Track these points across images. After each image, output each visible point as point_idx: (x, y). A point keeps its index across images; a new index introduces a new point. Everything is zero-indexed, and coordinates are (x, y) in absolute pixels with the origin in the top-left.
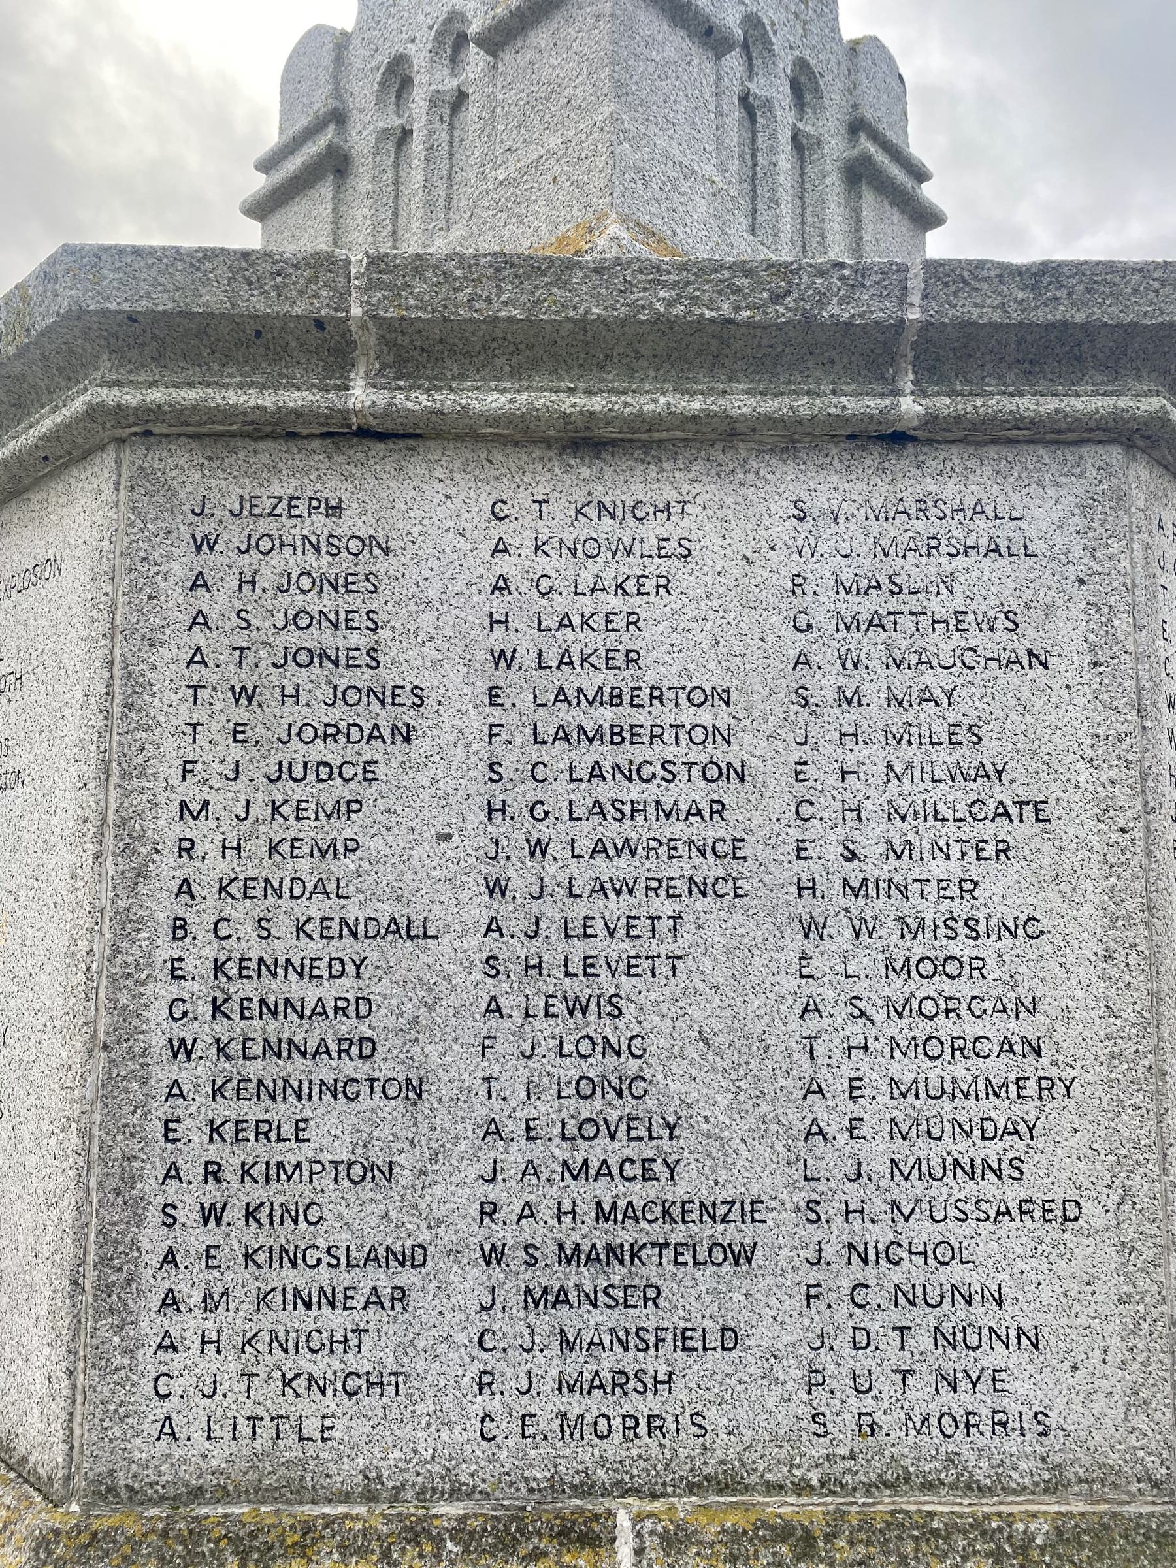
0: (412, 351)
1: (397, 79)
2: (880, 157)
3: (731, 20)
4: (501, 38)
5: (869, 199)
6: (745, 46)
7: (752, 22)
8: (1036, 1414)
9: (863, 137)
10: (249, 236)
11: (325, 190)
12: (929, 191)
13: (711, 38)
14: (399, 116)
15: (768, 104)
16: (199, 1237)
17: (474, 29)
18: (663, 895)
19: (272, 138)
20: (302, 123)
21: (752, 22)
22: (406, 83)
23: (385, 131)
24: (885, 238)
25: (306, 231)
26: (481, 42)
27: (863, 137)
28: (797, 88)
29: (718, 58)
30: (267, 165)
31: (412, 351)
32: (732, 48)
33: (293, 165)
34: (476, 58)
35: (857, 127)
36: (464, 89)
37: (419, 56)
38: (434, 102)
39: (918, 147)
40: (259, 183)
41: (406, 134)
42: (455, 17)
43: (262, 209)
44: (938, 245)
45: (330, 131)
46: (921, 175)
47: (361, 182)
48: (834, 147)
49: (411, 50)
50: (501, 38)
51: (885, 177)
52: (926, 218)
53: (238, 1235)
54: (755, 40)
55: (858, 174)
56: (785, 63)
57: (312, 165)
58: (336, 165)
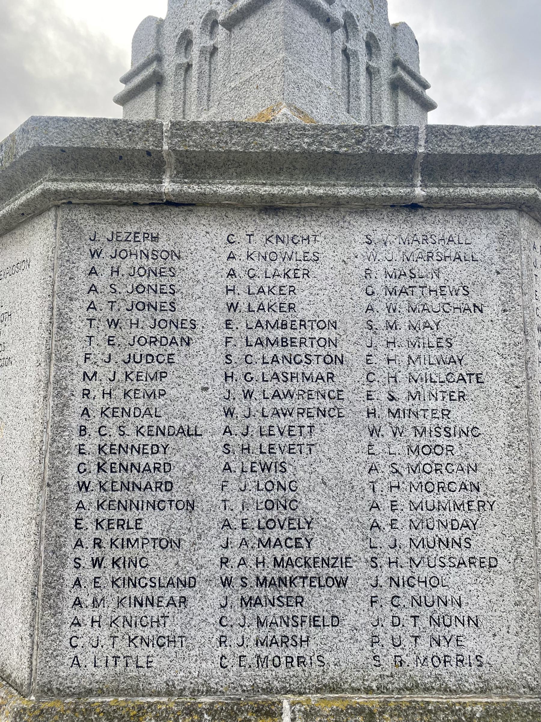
0: (192, 165)
1: (185, 41)
3: (337, 13)
4: (232, 23)
6: (345, 27)
7: (348, 16)
9: (399, 68)
10: (117, 112)
11: (152, 92)
12: (428, 93)
14: (186, 58)
15: (355, 53)
16: (91, 573)
17: (220, 18)
19: (128, 67)
20: (142, 61)
21: (348, 16)
24: (409, 115)
25: (144, 110)
26: (224, 24)
27: (399, 68)
28: (368, 46)
29: (332, 32)
30: (126, 80)
31: (192, 165)
32: (339, 27)
33: (137, 80)
34: (221, 31)
35: (396, 64)
36: (216, 46)
37: (196, 30)
38: (202, 51)
39: (424, 73)
40: (122, 88)
41: (189, 66)
42: (212, 13)
44: (433, 118)
45: (154, 65)
46: (425, 86)
47: (169, 88)
48: (386, 74)
49: (192, 28)
50: (232, 23)
51: (409, 87)
52: (428, 106)
53: (110, 572)
54: (349, 24)
55: (396, 85)
56: (363, 34)
57: (147, 80)
58: (158, 80)
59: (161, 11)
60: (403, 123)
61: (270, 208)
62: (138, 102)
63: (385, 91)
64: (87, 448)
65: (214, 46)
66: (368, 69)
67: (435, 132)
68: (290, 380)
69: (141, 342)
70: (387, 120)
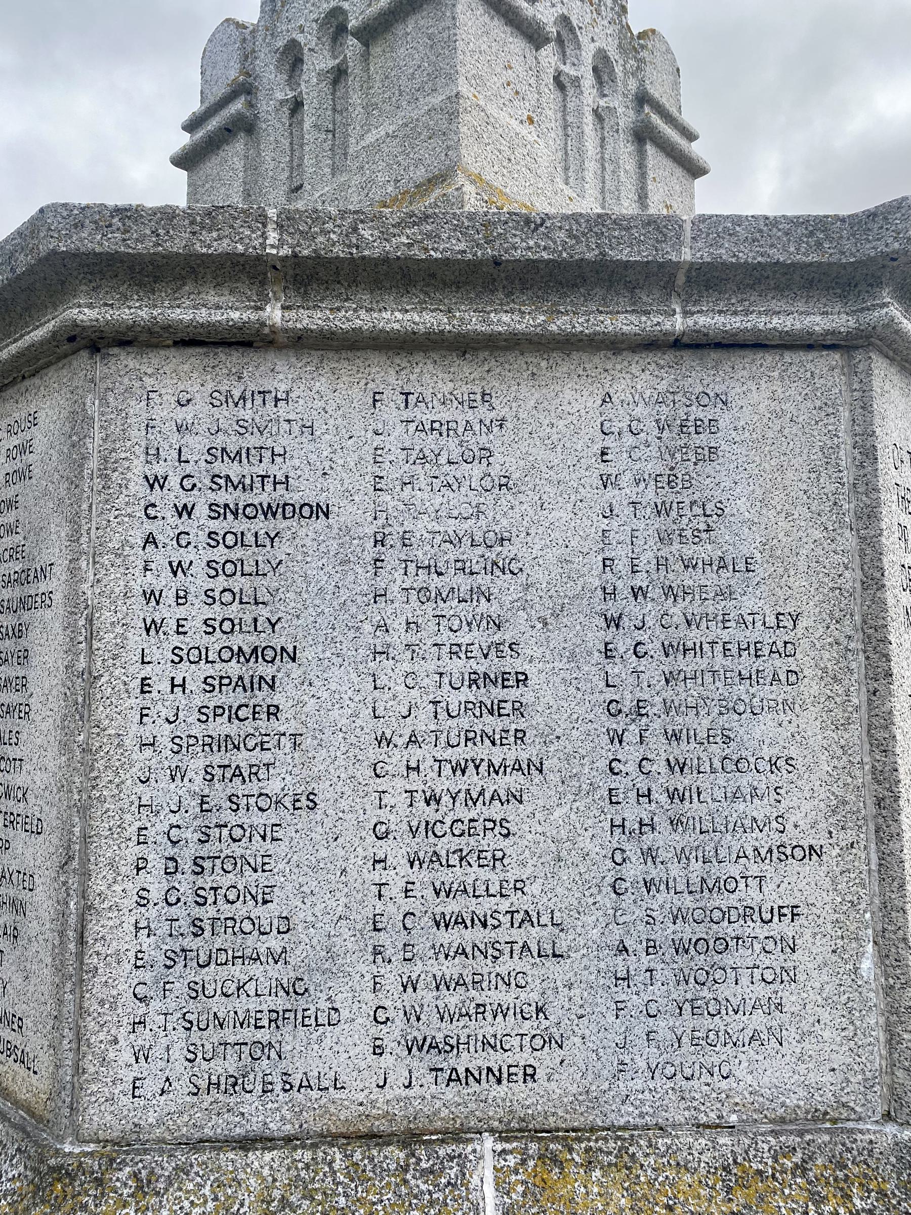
0: (309, 276)
1: (292, 58)
2: (656, 119)
3: (546, 15)
4: (373, 32)
5: (650, 149)
6: (560, 41)
8: (208, 562)
9: (647, 109)
10: (171, 189)
11: (237, 149)
12: (697, 149)
13: (534, 36)
14: (292, 90)
15: (576, 82)
17: (352, 23)
18: (463, 656)
19: (195, 106)
20: (220, 91)
22: (297, 62)
23: (282, 103)
24: (665, 193)
27: (647, 109)
30: (191, 126)
31: (309, 276)
32: (547, 40)
33: (213, 124)
35: (643, 99)
39: (687, 117)
40: (184, 139)
43: (186, 160)
44: (709, 199)
46: (691, 136)
48: (626, 117)
49: (300, 38)
50: (373, 32)
51: (657, 135)
54: (566, 35)
55: (643, 135)
58: (245, 126)
59: (250, 11)
60: (655, 208)
61: (462, 346)
62: (211, 166)
63: (625, 150)
64: (151, 833)
65: (339, 70)
66: (595, 112)
67: (712, 227)
68: (296, 1089)
69: (224, 628)
70: (627, 207)
